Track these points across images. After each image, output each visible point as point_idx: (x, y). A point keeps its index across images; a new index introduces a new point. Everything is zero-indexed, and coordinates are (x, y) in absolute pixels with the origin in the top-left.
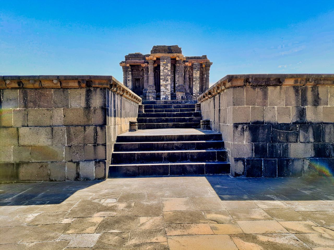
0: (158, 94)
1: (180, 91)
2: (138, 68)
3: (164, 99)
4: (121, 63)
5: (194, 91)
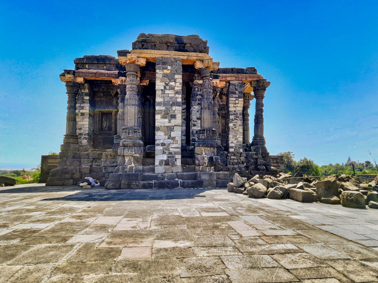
0: (149, 149)
1: (205, 144)
2: (108, 89)
3: (164, 163)
4: (63, 75)
5: (232, 143)
